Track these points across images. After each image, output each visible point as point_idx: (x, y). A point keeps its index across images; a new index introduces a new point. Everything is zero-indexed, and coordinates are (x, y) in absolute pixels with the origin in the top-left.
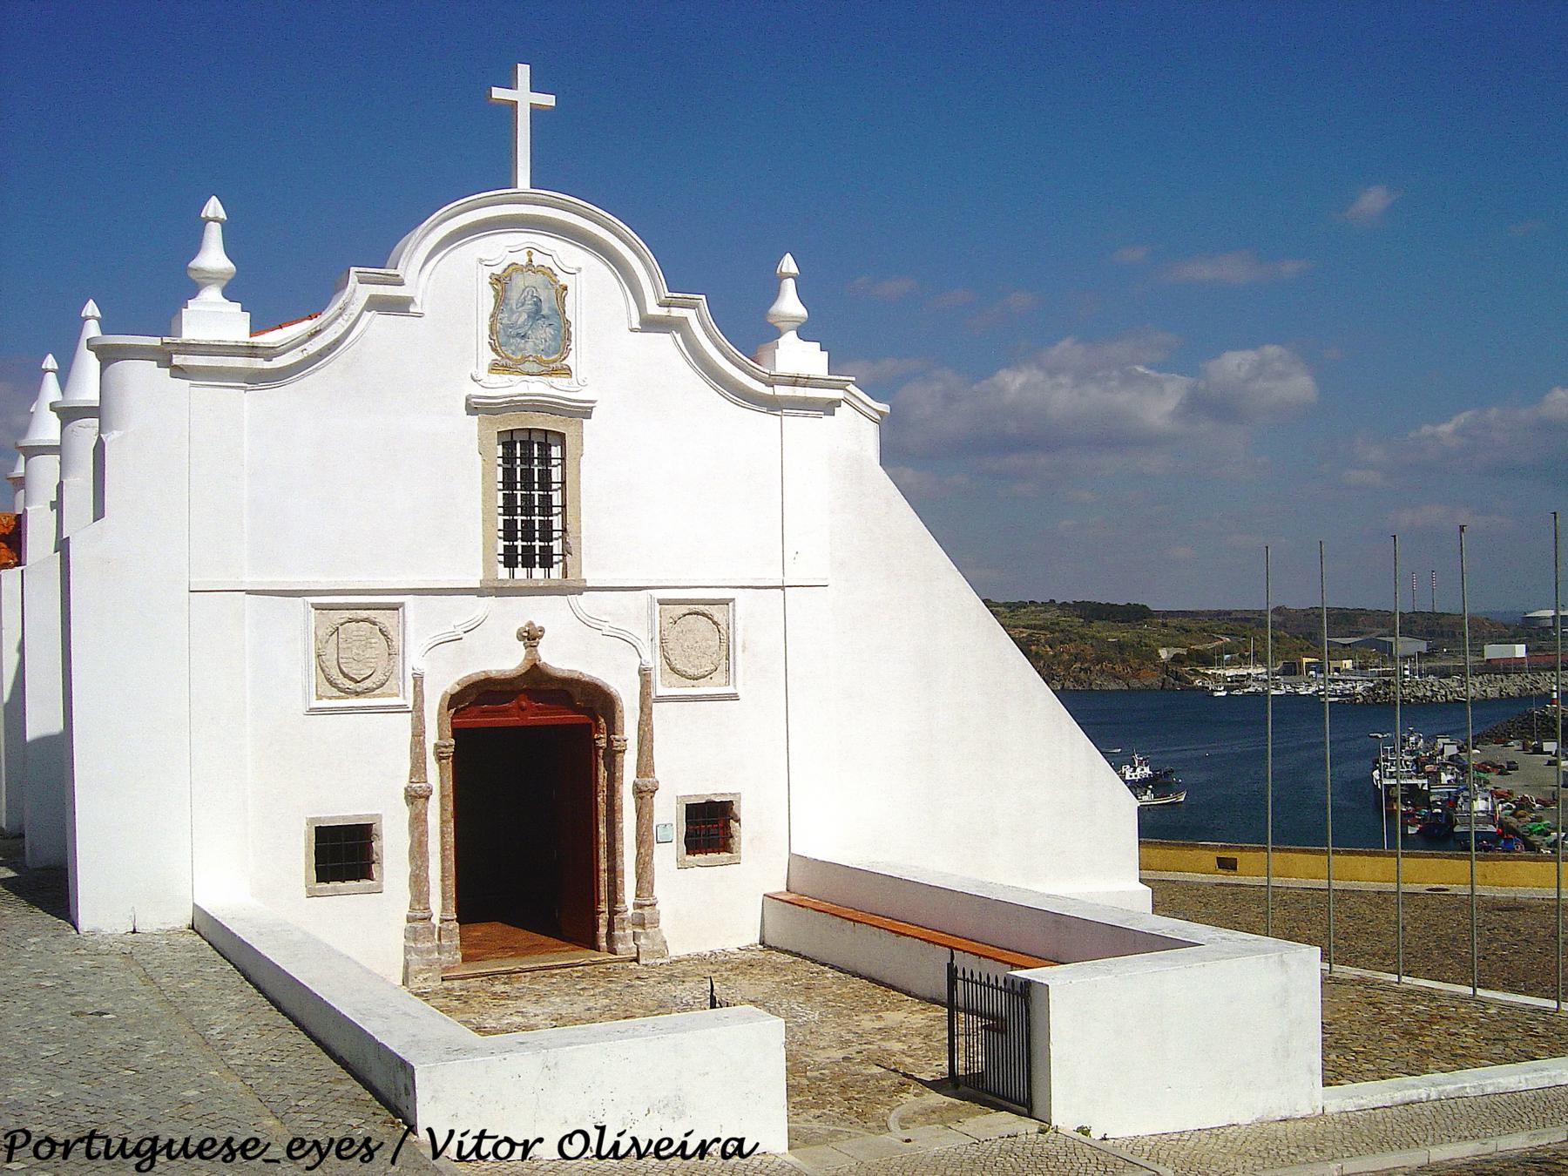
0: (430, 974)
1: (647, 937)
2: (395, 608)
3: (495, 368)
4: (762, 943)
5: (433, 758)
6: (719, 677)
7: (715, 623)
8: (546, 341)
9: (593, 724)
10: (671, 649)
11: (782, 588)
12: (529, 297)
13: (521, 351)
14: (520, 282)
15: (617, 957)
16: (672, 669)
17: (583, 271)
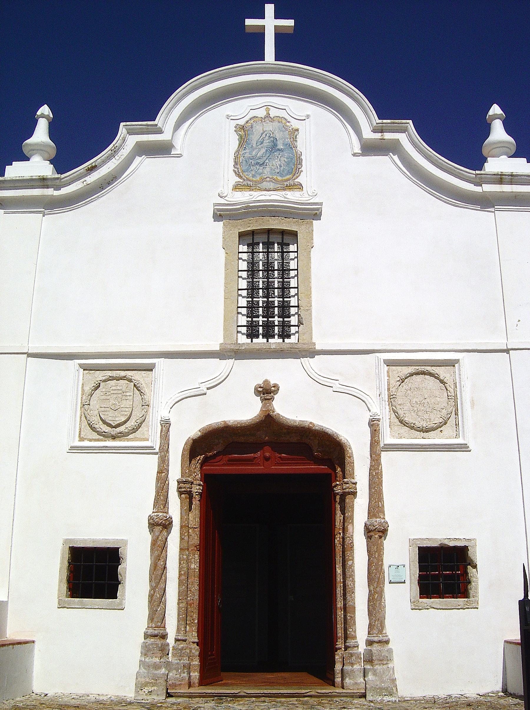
0: (155, 688)
1: (375, 674)
2: (150, 369)
3: (237, 187)
4: (505, 690)
5: (176, 494)
6: (447, 429)
7: (442, 382)
8: (281, 166)
9: (333, 474)
10: (400, 405)
11: (507, 351)
12: (267, 137)
13: (260, 174)
14: (258, 128)
15: (344, 691)
16: (401, 422)
17: (311, 118)
